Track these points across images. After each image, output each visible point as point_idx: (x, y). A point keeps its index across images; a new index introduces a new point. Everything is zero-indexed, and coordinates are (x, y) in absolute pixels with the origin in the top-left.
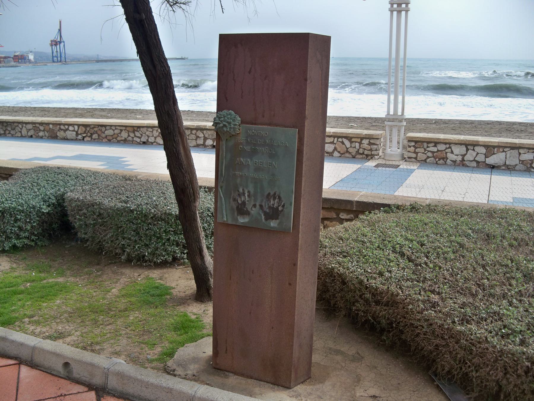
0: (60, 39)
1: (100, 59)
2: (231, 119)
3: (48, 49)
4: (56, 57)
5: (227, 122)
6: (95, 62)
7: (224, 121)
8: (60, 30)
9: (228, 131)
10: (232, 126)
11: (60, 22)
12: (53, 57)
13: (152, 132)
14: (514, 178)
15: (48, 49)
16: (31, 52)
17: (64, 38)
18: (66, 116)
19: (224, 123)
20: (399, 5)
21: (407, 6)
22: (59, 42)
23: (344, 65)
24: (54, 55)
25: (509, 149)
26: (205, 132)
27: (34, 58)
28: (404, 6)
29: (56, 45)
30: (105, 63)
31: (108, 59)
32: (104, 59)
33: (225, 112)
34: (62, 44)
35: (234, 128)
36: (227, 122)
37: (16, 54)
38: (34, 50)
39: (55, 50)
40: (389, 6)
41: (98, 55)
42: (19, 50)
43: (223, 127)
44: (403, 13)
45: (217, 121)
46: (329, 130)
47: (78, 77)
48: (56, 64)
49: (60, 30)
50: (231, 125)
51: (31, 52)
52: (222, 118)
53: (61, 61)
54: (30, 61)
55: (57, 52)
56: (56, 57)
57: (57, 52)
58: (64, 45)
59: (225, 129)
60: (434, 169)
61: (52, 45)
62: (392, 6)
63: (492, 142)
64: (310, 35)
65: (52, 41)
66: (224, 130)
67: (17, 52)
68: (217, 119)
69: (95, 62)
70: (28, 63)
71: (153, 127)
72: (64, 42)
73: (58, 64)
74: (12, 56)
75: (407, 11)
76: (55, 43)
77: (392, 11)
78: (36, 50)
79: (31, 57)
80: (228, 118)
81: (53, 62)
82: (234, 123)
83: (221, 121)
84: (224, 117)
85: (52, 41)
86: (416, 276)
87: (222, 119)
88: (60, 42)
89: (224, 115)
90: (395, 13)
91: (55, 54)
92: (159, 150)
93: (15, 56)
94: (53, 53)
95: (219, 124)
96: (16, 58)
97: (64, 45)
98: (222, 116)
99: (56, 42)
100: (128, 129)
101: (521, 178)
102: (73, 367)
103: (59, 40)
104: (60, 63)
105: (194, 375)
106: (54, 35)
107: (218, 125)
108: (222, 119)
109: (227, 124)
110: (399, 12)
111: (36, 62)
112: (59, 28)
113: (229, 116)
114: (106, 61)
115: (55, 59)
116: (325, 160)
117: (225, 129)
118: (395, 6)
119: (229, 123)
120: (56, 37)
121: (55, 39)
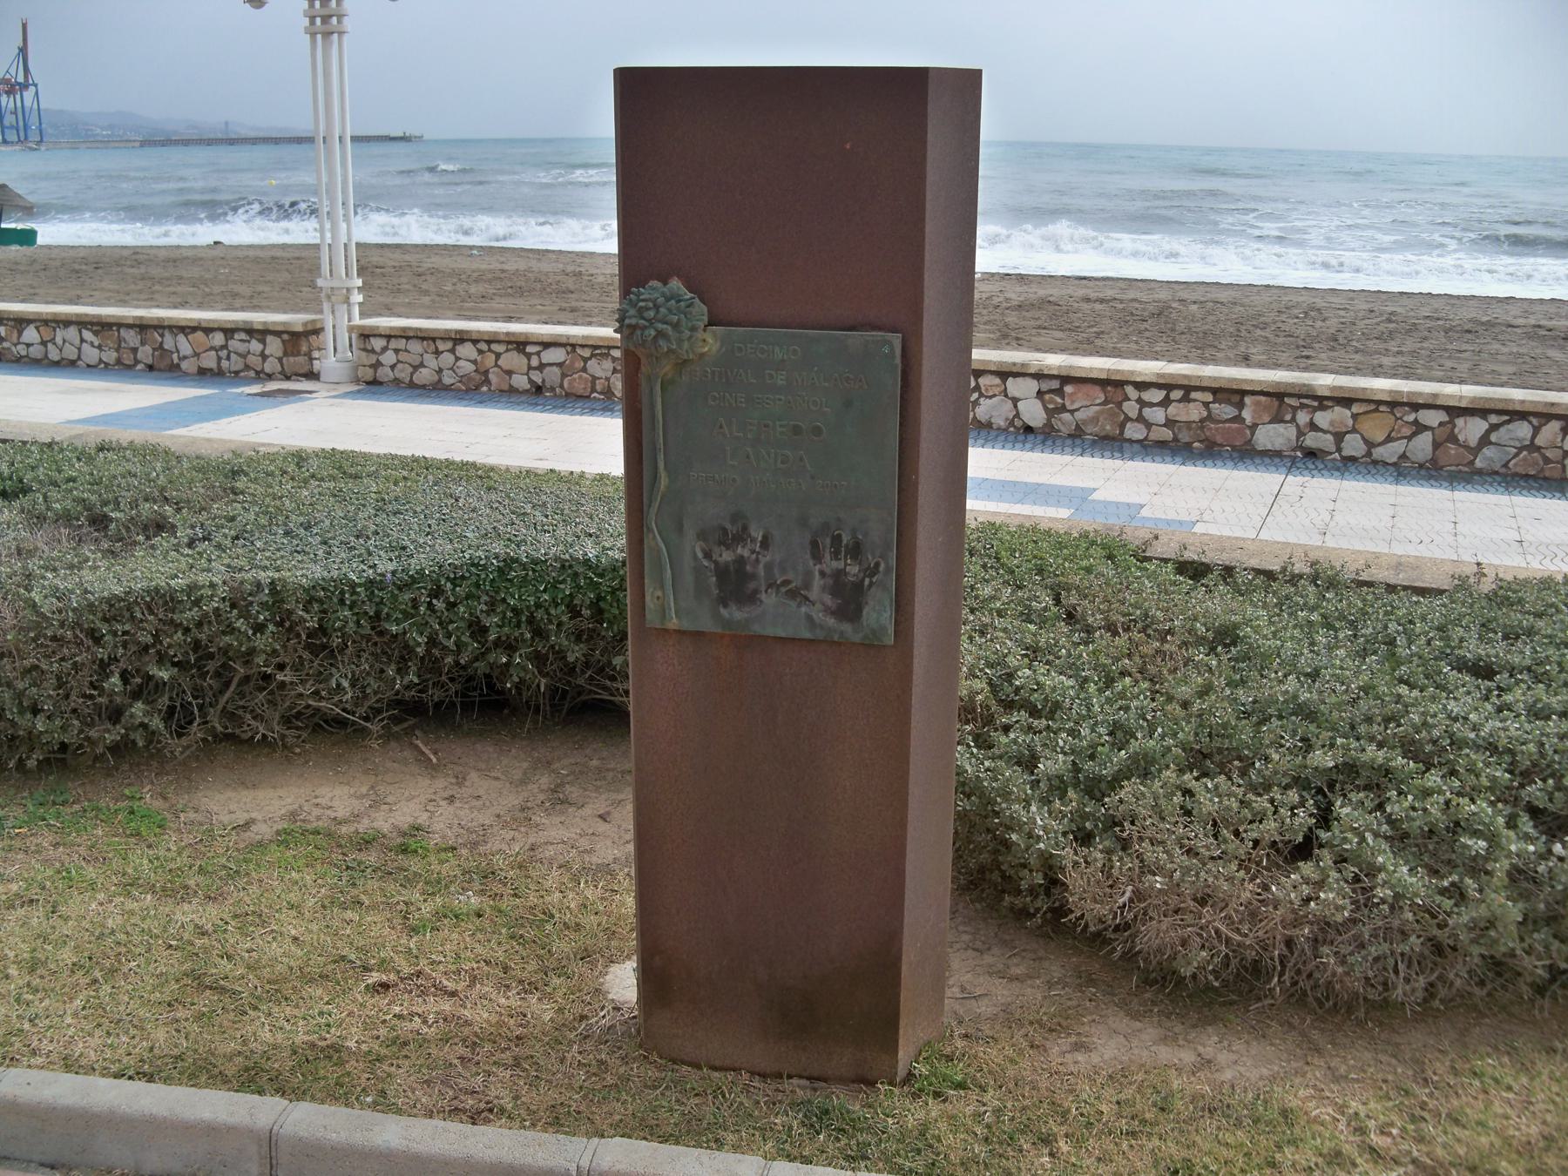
0: (26, 77)
1: (233, 136)
4: (12, 127)
8: (23, 51)
10: (688, 333)
11: (24, 26)
19: (660, 326)
23: (145, 143)
25: (1507, 418)
30: (249, 147)
31: (261, 135)
32: (252, 134)
33: (653, 290)
34: (32, 89)
44: (336, 36)
45: (633, 321)
47: (1486, 261)
49: (23, 51)
52: (650, 309)
58: (37, 93)
60: (1168, 459)
62: (312, 22)
64: (931, 74)
72: (36, 86)
75: (341, 33)
77: (313, 35)
87: (652, 314)
89: (654, 301)
95: (644, 328)
97: (37, 93)
98: (651, 305)
102: (410, 820)
107: (639, 332)
108: (652, 314)
110: (327, 34)
113: (673, 302)
114: (255, 141)
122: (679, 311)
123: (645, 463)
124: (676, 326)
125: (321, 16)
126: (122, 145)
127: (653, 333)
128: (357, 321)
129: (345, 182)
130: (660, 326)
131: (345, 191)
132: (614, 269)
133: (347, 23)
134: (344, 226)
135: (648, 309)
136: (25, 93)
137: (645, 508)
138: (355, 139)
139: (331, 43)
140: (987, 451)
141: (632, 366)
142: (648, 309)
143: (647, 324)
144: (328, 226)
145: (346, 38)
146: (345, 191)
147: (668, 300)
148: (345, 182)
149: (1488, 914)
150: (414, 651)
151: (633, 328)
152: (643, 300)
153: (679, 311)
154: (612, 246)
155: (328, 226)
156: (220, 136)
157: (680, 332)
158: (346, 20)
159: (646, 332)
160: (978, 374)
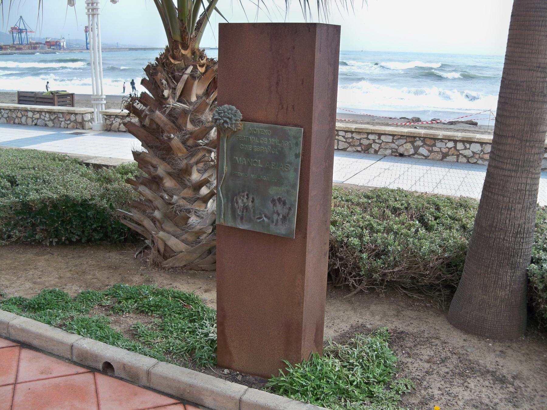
2: (232, 114)
5: (228, 118)
7: (224, 117)
10: (234, 122)
19: (225, 119)
35: (235, 124)
36: (228, 118)
37: (48, 40)
40: (86, 11)
41: (117, 43)
46: (338, 125)
50: (232, 121)
52: (222, 113)
59: (226, 125)
62: (88, 11)
66: (224, 127)
67: (49, 38)
68: (216, 114)
74: (44, 43)
75: (98, 14)
77: (89, 15)
80: (228, 114)
82: (235, 118)
86: (156, 285)
87: (222, 115)
89: (223, 110)
90: (91, 15)
93: (47, 42)
95: (220, 119)
96: (48, 44)
98: (222, 112)
105: (110, 396)
107: (218, 121)
108: (222, 115)
109: (228, 120)
110: (93, 15)
113: (230, 111)
116: (335, 155)
117: (226, 125)
119: (230, 119)
124: (230, 119)
125: (92, 15)
126: (118, 50)
127: (222, 121)
128: (104, 110)
129: (99, 57)
130: (225, 119)
131: (99, 60)
133: (99, 11)
134: (99, 81)
135: (222, 113)
138: (104, 49)
140: (339, 158)
142: (222, 113)
143: (220, 118)
144: (94, 79)
145: (99, 16)
146: (99, 60)
147: (228, 110)
148: (99, 57)
151: (216, 119)
152: (220, 110)
155: (94, 79)
156: (115, 47)
158: (99, 4)
159: (221, 121)
160: (337, 131)
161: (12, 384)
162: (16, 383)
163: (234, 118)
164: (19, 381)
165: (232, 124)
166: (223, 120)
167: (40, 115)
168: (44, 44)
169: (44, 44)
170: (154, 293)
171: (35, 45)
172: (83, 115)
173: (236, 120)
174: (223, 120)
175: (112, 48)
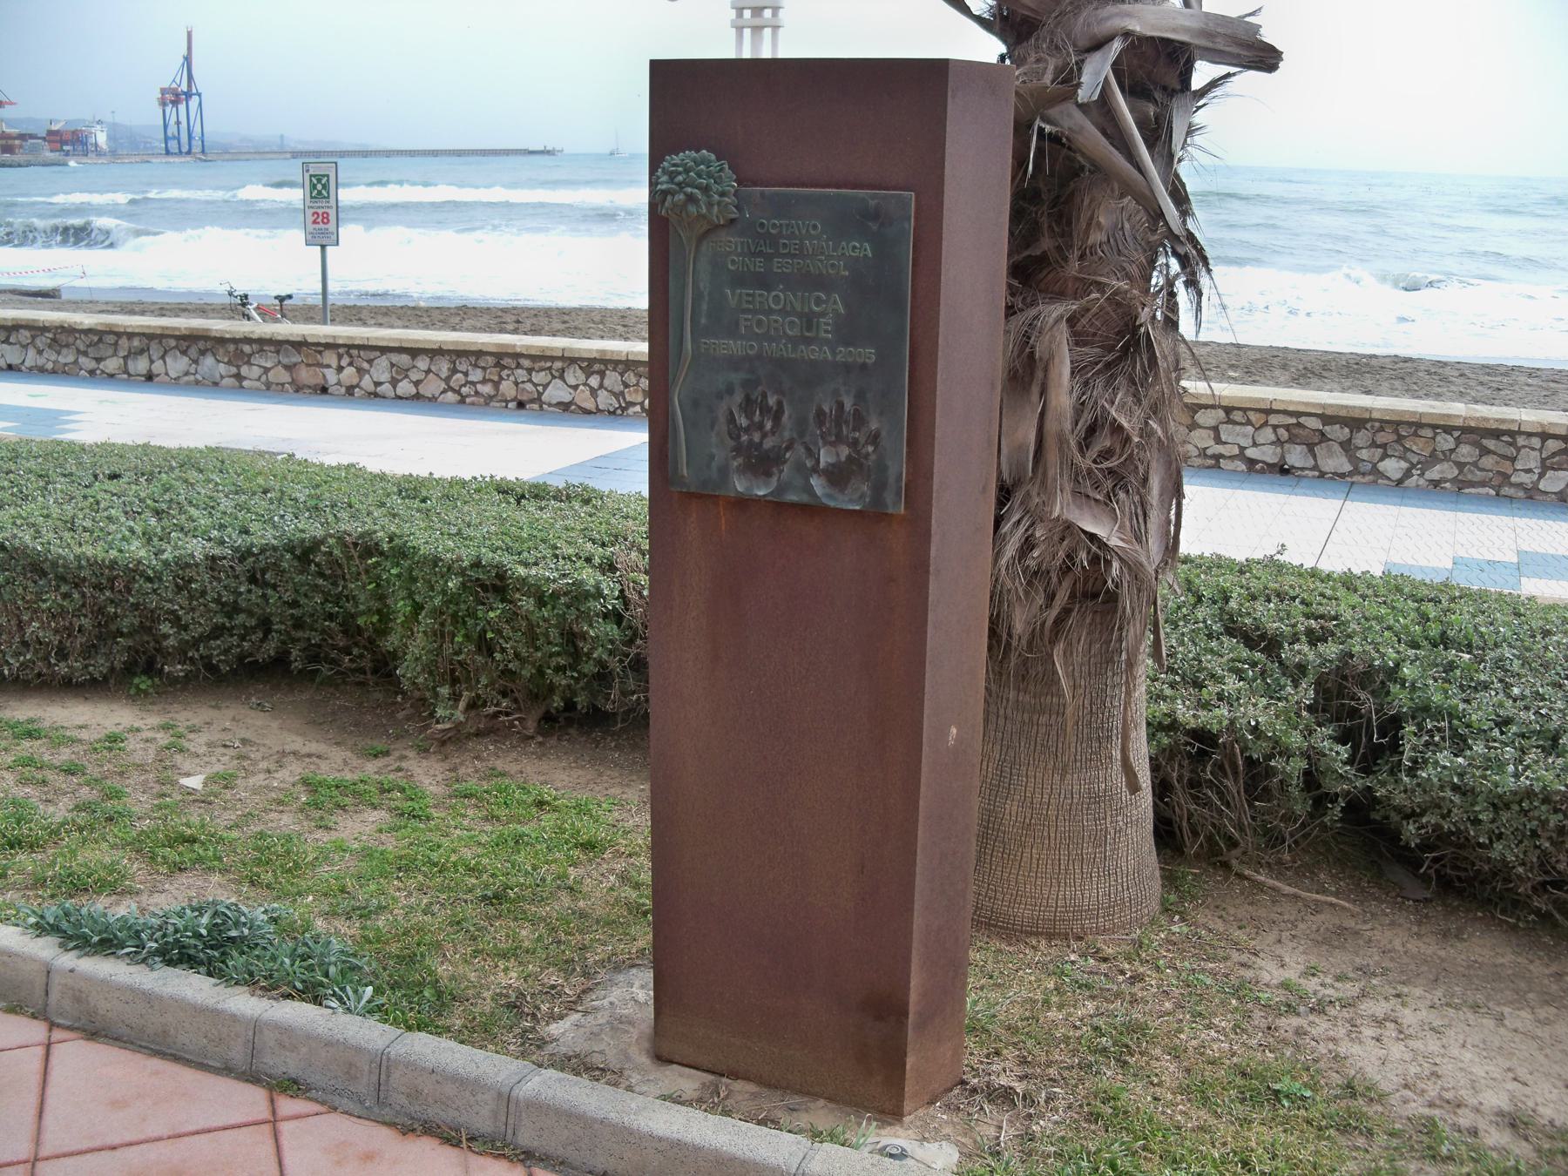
0: (189, 86)
3: (146, 115)
4: (174, 138)
6: (289, 156)
7: (688, 185)
8: (188, 59)
9: (704, 217)
10: (716, 197)
11: (189, 35)
12: (166, 139)
13: (1434, 438)
14: (1406, 510)
15: (146, 115)
16: (100, 122)
17: (200, 83)
18: (536, 331)
19: (689, 190)
20: (758, 11)
21: (775, 14)
22: (185, 93)
24: (169, 134)
26: (1249, 413)
27: (109, 138)
28: (768, 13)
29: (175, 103)
34: (195, 99)
37: (55, 127)
38: (108, 118)
39: (174, 119)
40: (733, 14)
41: (282, 136)
42: (58, 111)
43: (684, 205)
44: (767, 32)
48: (177, 160)
49: (188, 59)
51: (100, 122)
52: (680, 173)
53: (189, 152)
54: (98, 152)
55: (178, 123)
56: (174, 138)
57: (178, 123)
60: (1237, 484)
61: (163, 103)
63: (383, 339)
65: (163, 91)
67: (57, 121)
69: (289, 156)
70: (93, 155)
71: (626, 365)
72: (199, 95)
73: (183, 160)
75: (776, 28)
76: (174, 97)
77: (739, 29)
78: (118, 119)
79: (102, 138)
81: (168, 153)
83: (679, 184)
84: (687, 171)
85: (163, 91)
87: (680, 178)
88: (188, 95)
90: (747, 32)
91: (172, 130)
92: (624, 430)
93: (50, 133)
94: (165, 126)
95: (673, 194)
96: (52, 138)
98: (680, 169)
99: (177, 95)
100: (1274, 420)
101: (1541, 522)
103: (184, 87)
104: (188, 159)
106: (169, 74)
107: (669, 198)
108: (680, 178)
111: (114, 154)
112: (185, 52)
115: (173, 145)
117: (692, 209)
118: (747, 14)
119: (706, 189)
120: (178, 81)
121: (174, 86)
122: (710, 175)
123: (672, 315)
124: (706, 189)
130: (689, 190)
132: (646, 314)
136: (190, 103)
137: (671, 377)
139: (761, 39)
141: (659, 366)
147: (697, 164)
149: (1512, 1108)
150: (1270, 772)
153: (710, 175)
154: (647, 350)
156: (275, 149)
157: (709, 196)
158: (781, 13)
161: (25, 1162)
162: (36, 1160)
163: (715, 187)
164: (44, 1152)
165: (710, 205)
166: (685, 194)
167: (33, 337)
168: (44, 139)
169: (44, 139)
170: (1516, 904)
171: (10, 142)
172: (267, 1128)
173: (722, 194)
174: (685, 194)
175: (267, 149)
